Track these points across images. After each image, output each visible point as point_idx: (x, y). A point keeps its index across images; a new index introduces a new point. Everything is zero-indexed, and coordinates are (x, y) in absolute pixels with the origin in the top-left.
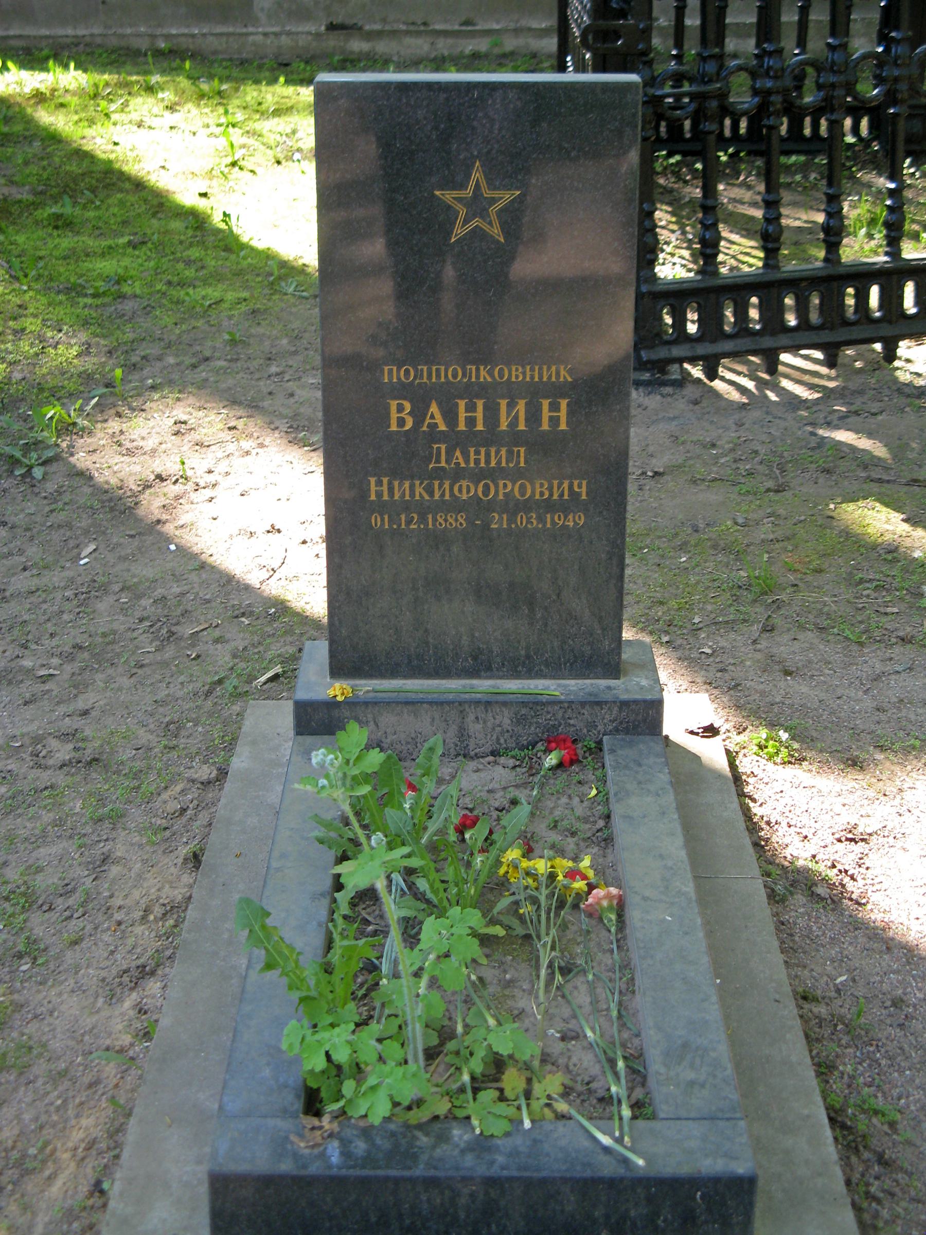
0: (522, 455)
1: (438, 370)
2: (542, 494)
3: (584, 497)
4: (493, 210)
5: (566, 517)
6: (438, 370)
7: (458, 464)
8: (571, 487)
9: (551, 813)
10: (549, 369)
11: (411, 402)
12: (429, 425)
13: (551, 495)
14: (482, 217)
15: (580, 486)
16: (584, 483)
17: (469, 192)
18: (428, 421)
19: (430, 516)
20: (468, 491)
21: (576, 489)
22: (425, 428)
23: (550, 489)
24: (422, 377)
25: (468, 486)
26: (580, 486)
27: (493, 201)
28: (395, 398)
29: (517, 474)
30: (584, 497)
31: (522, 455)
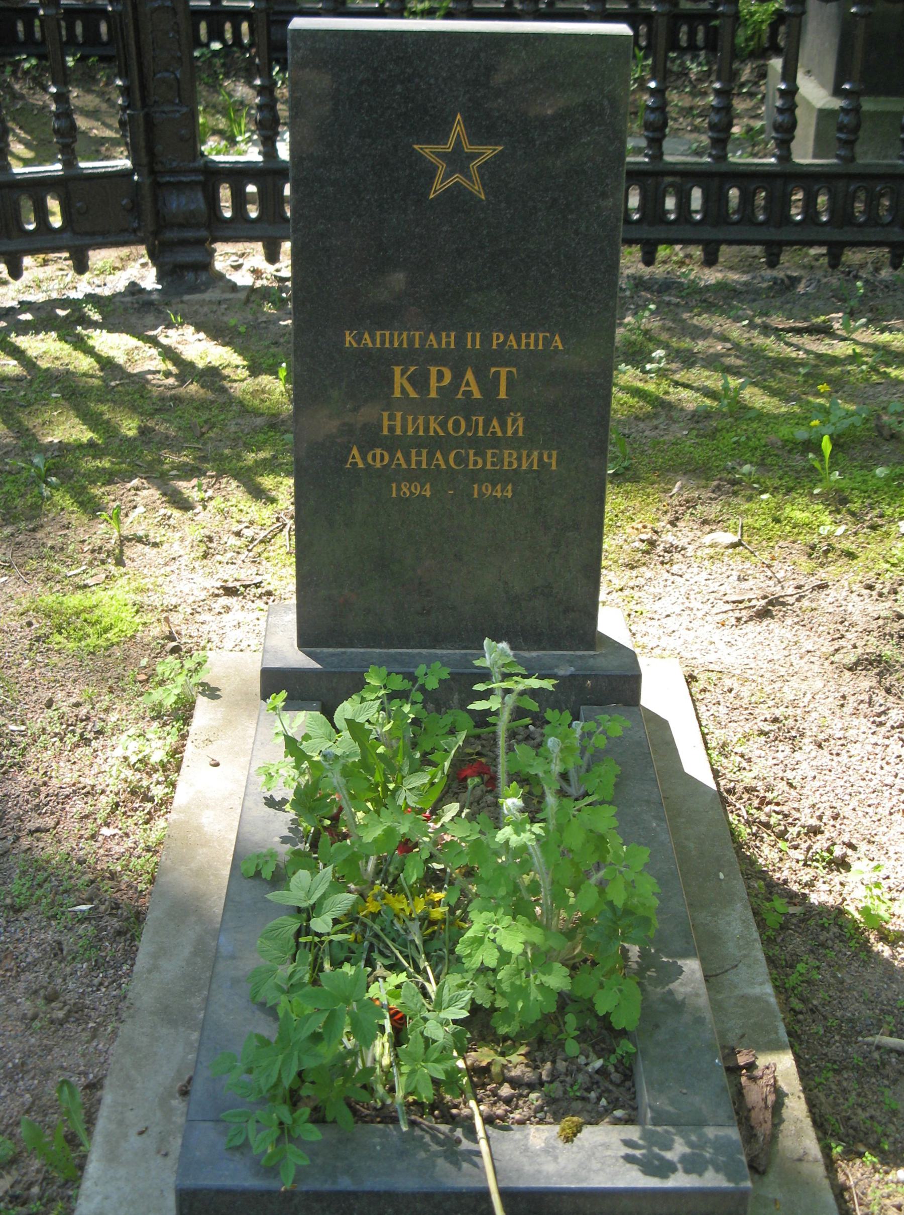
0: (481, 425)
1: (383, 336)
2: (510, 464)
3: (554, 467)
4: (442, 168)
5: (422, 488)
6: (383, 336)
7: (494, 433)
8: (540, 459)
9: (96, 776)
10: (400, 335)
11: (451, 369)
12: (464, 393)
13: (520, 466)
14: (461, 172)
15: (550, 457)
16: (554, 453)
17: (468, 148)
18: (463, 389)
19: (394, 485)
20: (382, 460)
21: (546, 460)
22: (460, 396)
23: (519, 459)
24: (545, 338)
25: (382, 455)
26: (550, 457)
27: (473, 156)
28: (436, 365)
29: (515, 443)
30: (554, 467)
31: (481, 425)
